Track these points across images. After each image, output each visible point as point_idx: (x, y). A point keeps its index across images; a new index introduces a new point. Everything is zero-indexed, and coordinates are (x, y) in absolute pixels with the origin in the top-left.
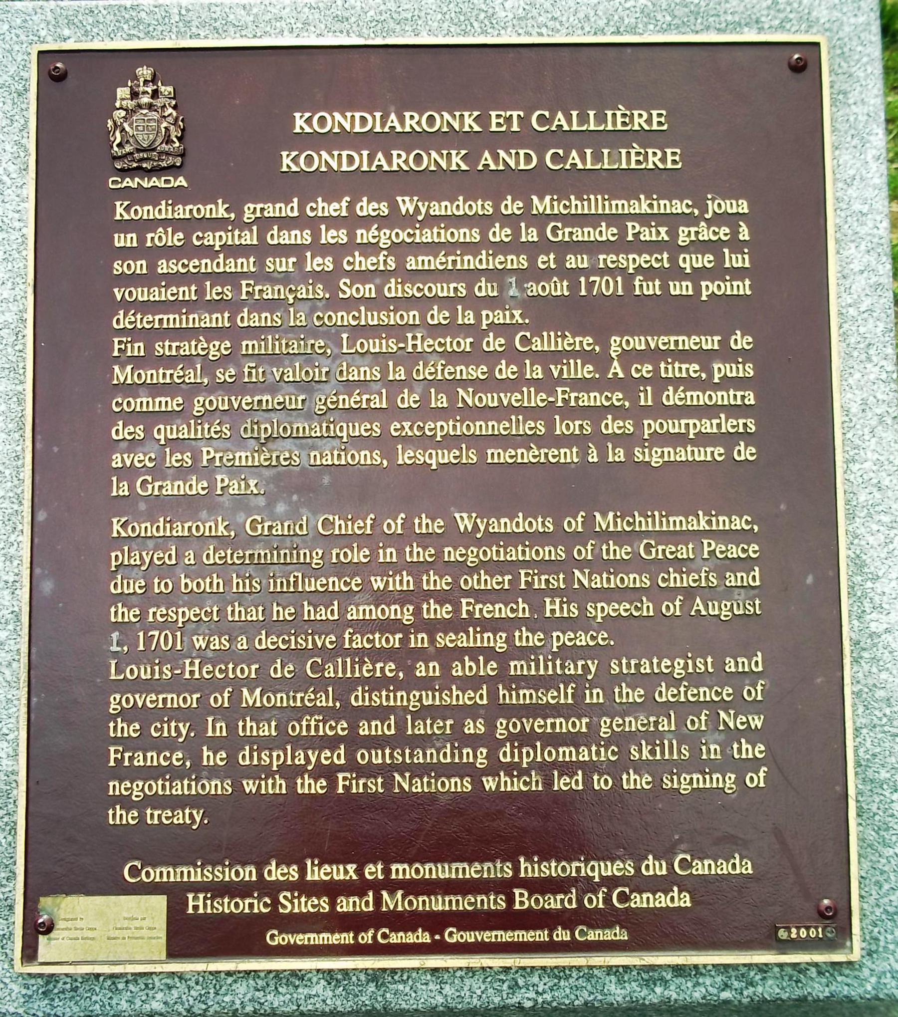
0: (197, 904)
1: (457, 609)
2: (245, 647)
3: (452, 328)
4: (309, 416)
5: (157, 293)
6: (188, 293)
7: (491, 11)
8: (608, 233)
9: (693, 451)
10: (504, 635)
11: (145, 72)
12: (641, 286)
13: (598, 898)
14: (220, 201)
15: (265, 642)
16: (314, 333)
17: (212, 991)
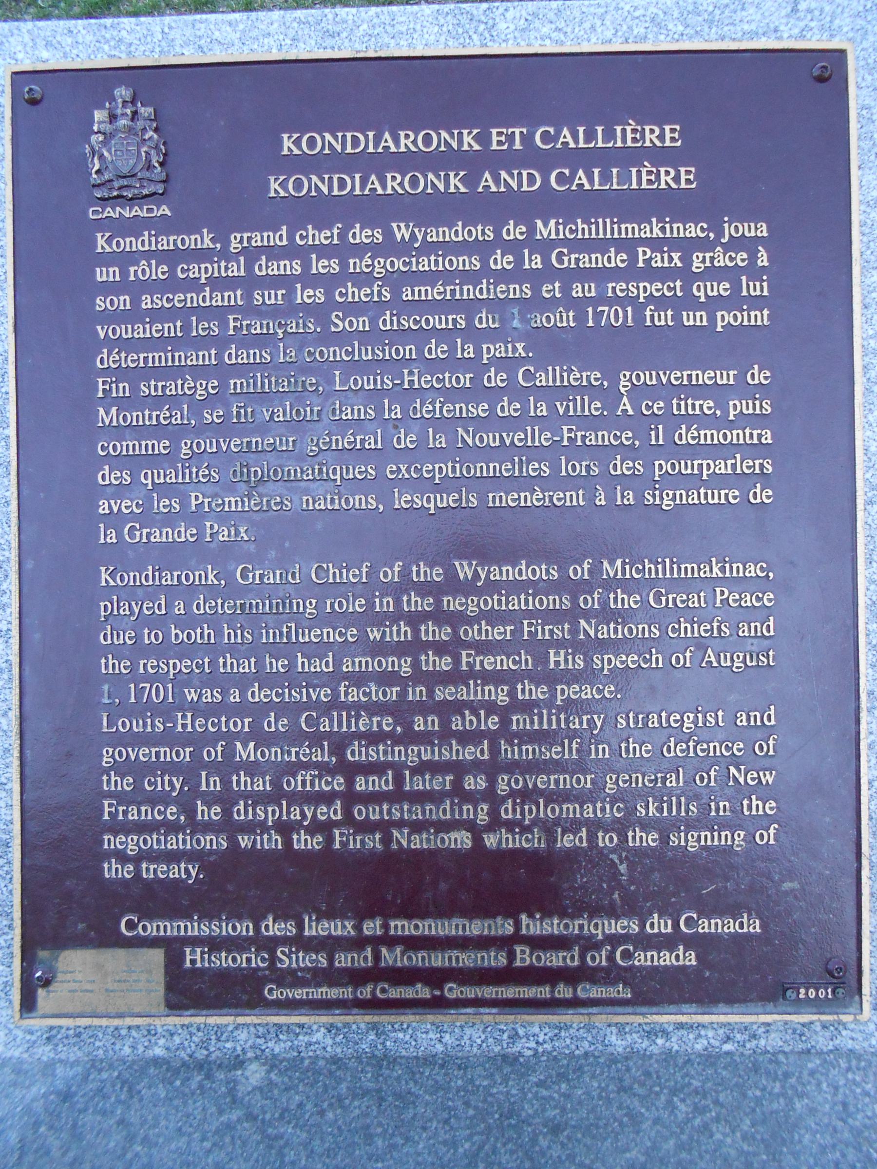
0: (194, 957)
1: (457, 660)
2: (238, 700)
3: (453, 363)
4: (302, 458)
5: (141, 330)
6: (172, 329)
7: (491, 22)
8: (618, 260)
9: (706, 494)
10: (506, 688)
11: (122, 93)
12: (652, 316)
13: (601, 956)
14: (205, 231)
15: (258, 695)
16: (306, 370)
17: (213, 1037)
